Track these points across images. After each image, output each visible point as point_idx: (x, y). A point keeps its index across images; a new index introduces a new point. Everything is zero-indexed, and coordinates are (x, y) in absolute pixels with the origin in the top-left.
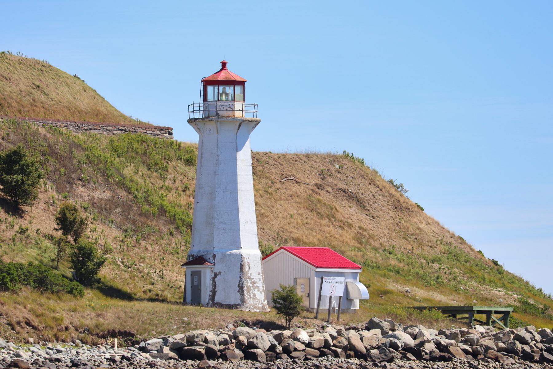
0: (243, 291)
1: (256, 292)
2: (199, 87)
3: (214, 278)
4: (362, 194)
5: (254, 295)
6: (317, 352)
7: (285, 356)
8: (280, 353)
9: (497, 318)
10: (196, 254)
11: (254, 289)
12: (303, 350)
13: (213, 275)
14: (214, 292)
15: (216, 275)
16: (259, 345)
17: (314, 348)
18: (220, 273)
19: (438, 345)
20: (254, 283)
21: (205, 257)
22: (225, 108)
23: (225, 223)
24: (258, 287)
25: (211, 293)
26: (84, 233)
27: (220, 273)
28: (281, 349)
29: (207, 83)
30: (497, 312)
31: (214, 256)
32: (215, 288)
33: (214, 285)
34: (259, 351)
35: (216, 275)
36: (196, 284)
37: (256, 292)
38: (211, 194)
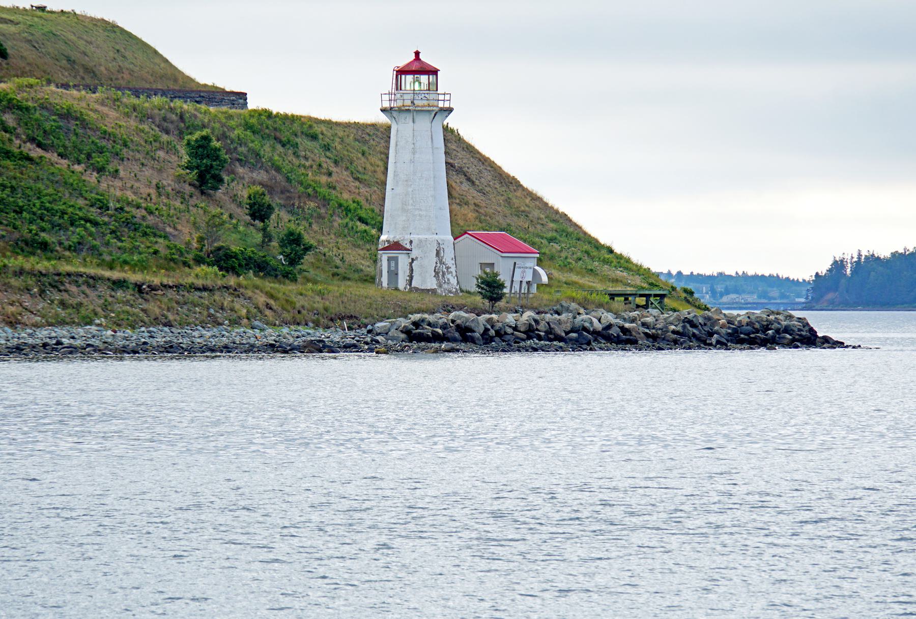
0: (439, 276)
1: (449, 276)
2: (390, 76)
3: (411, 264)
4: (468, 168)
5: (448, 280)
6: (523, 336)
7: (497, 339)
8: (493, 337)
9: (253, 237)
10: (391, 240)
11: (449, 274)
12: (512, 334)
13: (410, 261)
14: (411, 277)
15: (413, 260)
16: (476, 329)
17: (520, 331)
18: (417, 258)
19: (622, 329)
20: (448, 268)
21: (401, 242)
22: (420, 97)
23: (421, 210)
24: (451, 272)
25: (408, 278)
26: (662, 278)
27: (417, 258)
28: (494, 332)
29: (401, 72)
30: (656, 295)
31: (411, 242)
32: (412, 273)
33: (412, 270)
34: (477, 335)
35: (413, 260)
36: (393, 269)
37: (449, 276)
38: (406, 181)
